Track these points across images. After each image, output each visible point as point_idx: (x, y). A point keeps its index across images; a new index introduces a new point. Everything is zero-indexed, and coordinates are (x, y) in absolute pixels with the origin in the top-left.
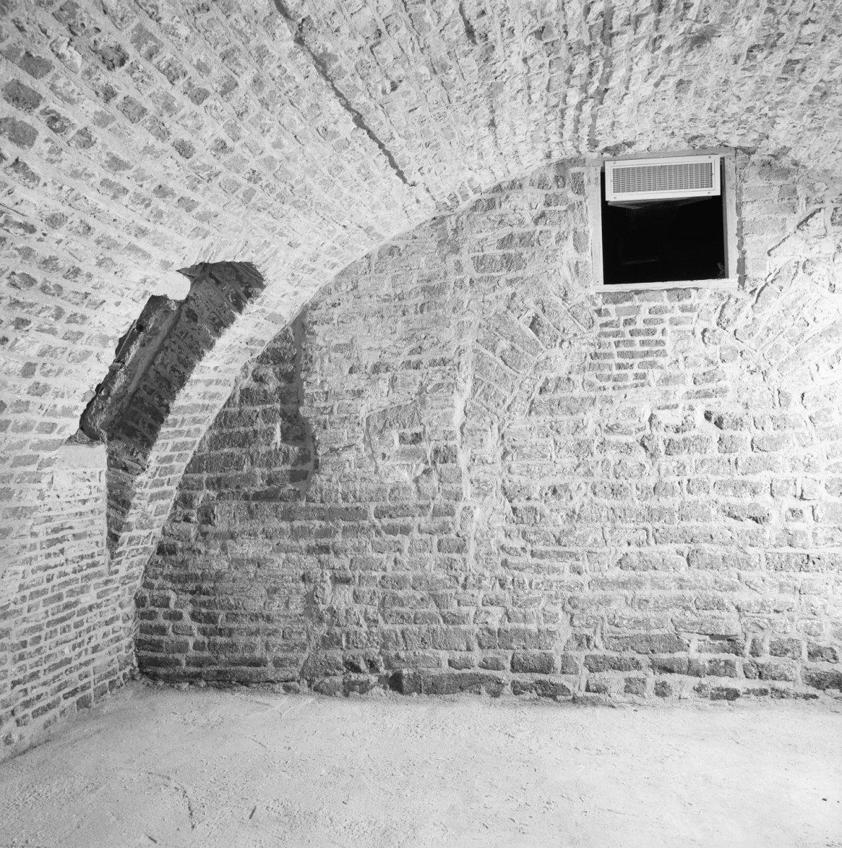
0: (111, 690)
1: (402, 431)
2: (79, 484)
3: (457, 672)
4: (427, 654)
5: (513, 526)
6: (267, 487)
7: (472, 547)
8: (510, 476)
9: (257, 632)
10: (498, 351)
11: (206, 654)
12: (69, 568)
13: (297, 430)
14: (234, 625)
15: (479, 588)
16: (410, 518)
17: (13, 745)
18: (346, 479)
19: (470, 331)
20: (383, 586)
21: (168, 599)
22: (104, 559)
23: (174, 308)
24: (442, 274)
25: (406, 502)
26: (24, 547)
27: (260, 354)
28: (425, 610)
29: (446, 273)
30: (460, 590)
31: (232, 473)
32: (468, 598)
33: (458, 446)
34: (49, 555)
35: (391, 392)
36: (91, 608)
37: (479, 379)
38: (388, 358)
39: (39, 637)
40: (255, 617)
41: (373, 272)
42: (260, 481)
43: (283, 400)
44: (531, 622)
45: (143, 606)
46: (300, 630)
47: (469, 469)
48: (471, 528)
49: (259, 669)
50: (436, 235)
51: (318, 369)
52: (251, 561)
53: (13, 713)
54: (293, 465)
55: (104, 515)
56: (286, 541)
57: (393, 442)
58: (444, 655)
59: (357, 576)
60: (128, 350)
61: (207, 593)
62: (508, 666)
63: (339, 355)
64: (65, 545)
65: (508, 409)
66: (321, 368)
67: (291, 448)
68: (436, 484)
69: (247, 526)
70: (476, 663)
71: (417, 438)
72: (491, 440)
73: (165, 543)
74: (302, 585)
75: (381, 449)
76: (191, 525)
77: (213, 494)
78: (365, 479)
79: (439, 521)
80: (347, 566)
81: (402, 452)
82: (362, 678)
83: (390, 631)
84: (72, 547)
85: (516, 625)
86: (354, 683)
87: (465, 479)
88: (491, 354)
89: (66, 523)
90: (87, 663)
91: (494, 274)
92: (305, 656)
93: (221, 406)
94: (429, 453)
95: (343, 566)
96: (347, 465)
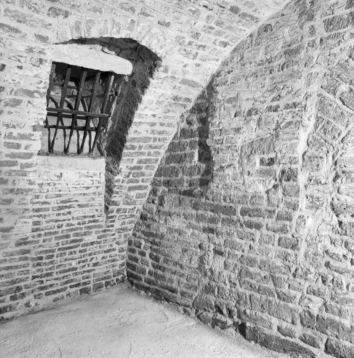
0: (106, 286)
1: (262, 156)
2: (84, 178)
3: (282, 337)
4: (264, 317)
5: (338, 236)
6: (189, 188)
7: (303, 247)
8: (338, 195)
9: (175, 273)
10: (338, 94)
11: (153, 278)
12: (75, 222)
13: (206, 155)
14: (166, 266)
15: (306, 279)
16: (262, 218)
17: (31, 308)
18: (226, 187)
19: (317, 80)
20: (241, 262)
21: (141, 244)
22: (103, 218)
23: (127, 79)
24: (299, 39)
25: (260, 207)
26: (27, 210)
27: (191, 107)
28: (266, 285)
29: (302, 37)
30: (291, 277)
31: (174, 178)
32: (296, 285)
33: (299, 169)
34: (59, 214)
35: (258, 128)
36: (92, 243)
37: (320, 117)
38: (258, 105)
39: (53, 256)
40: (176, 264)
41: (253, 46)
42: (186, 184)
43: (200, 137)
44: (345, 317)
45: (131, 245)
46: (195, 278)
47: (306, 187)
48: (304, 232)
49: (173, 294)
50: (298, 9)
51: (217, 115)
52: (177, 231)
53: (32, 292)
54: (202, 176)
55: (103, 196)
56: (193, 222)
57: (255, 164)
58: (275, 322)
59: (227, 251)
60: (112, 107)
61: (156, 245)
62: (323, 347)
63: (229, 105)
64: (72, 210)
65: (342, 141)
66: (219, 115)
67: (202, 165)
68: (281, 196)
69: (177, 210)
70: (297, 335)
71: (272, 161)
72: (326, 165)
73: (143, 213)
74: (199, 250)
75: (247, 168)
76: (155, 205)
77: (166, 189)
78: (237, 188)
79: (280, 224)
80: (222, 244)
81: (261, 171)
82: (223, 319)
83: (243, 293)
84: (77, 211)
85: (332, 316)
86: (219, 321)
87: (302, 195)
88: (332, 97)
89: (72, 198)
90: (89, 271)
91: (340, 31)
92: (197, 294)
93: (171, 139)
94: (278, 173)
95: (220, 244)
96: (228, 178)
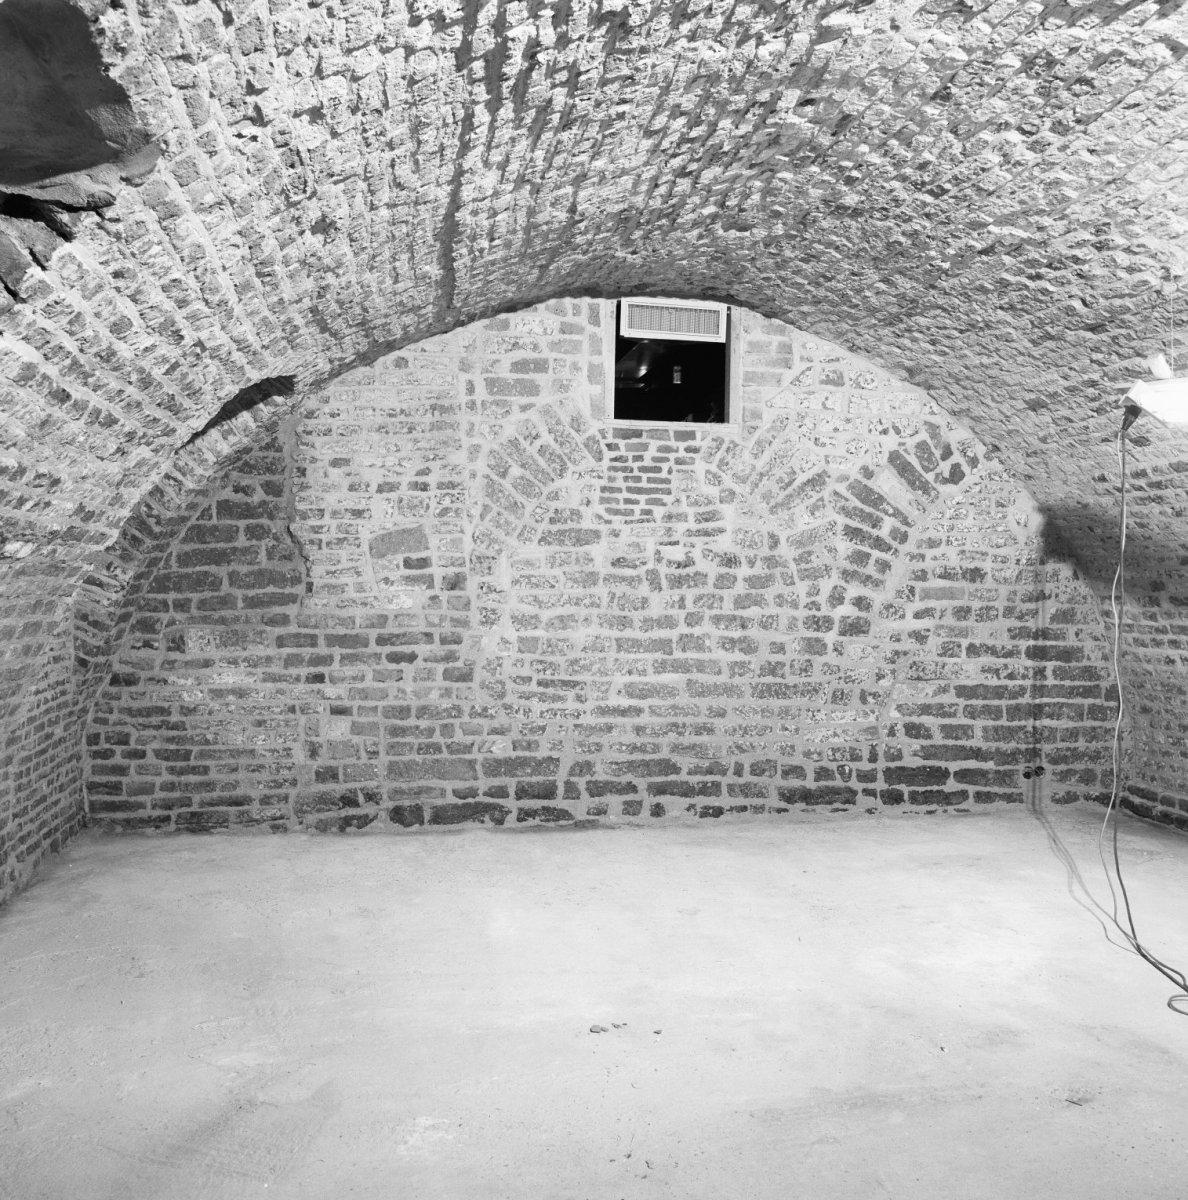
7: (479, 675)
52: (233, 692)
